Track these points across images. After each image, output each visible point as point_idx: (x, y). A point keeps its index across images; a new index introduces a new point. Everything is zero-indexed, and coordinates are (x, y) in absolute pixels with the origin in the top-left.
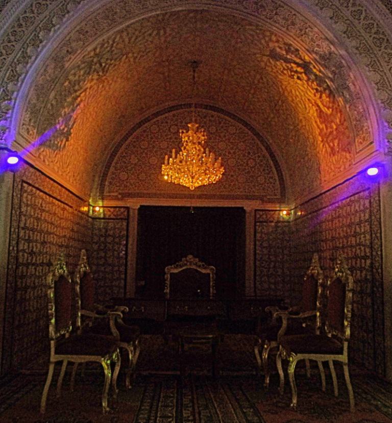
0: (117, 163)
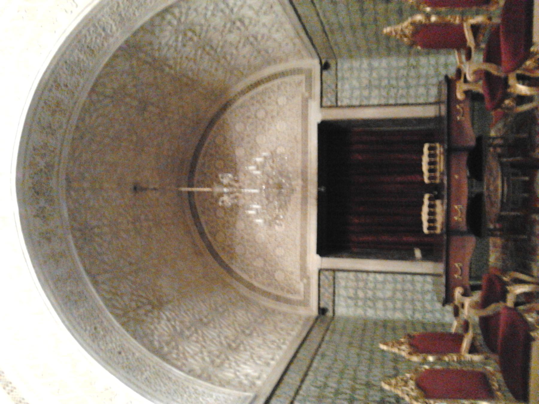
0: (263, 284)
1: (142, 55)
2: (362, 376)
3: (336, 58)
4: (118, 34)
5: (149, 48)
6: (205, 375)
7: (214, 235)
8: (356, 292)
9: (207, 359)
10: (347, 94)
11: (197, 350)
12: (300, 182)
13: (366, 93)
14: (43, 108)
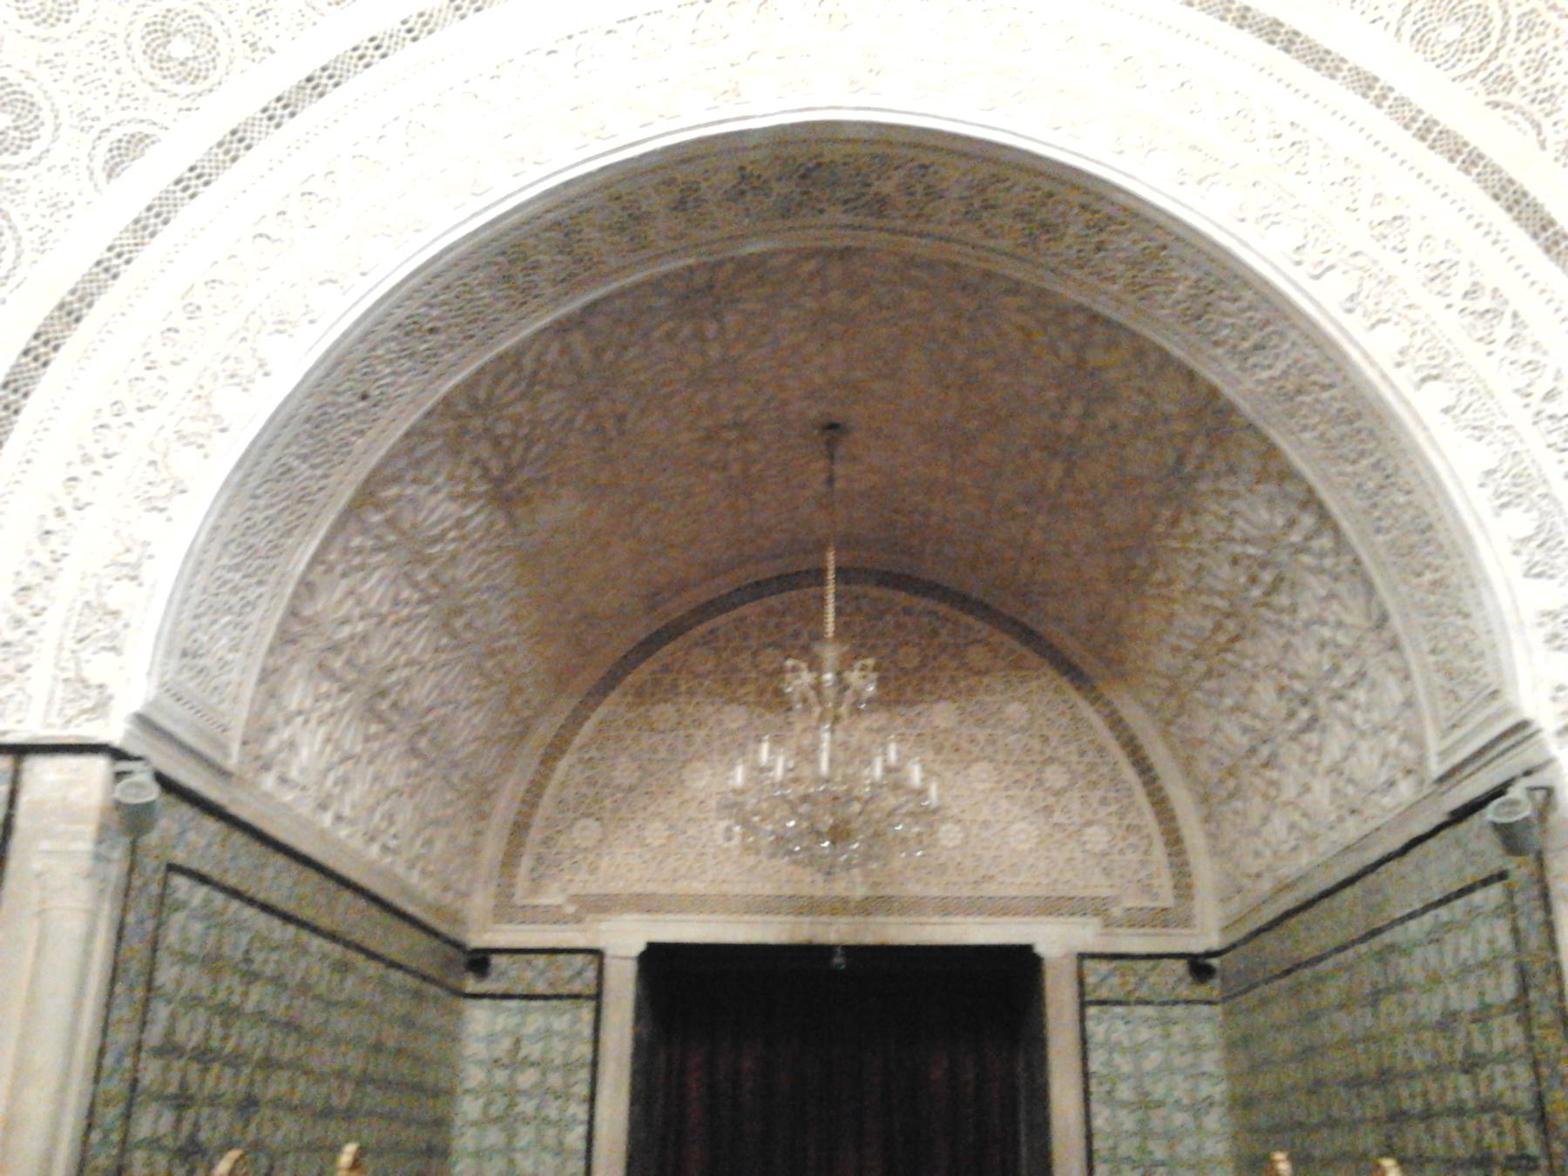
0: (563, 785)
1: (1199, 448)
2: (278, 1086)
3: (1224, 1000)
4: (1248, 384)
5: (1219, 464)
6: (296, 628)
7: (708, 640)
8: (532, 1064)
9: (346, 631)
10: (1120, 1032)
11: (372, 604)
12: (860, 892)
13: (1125, 1092)
14: (1037, 189)
